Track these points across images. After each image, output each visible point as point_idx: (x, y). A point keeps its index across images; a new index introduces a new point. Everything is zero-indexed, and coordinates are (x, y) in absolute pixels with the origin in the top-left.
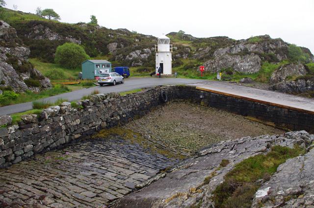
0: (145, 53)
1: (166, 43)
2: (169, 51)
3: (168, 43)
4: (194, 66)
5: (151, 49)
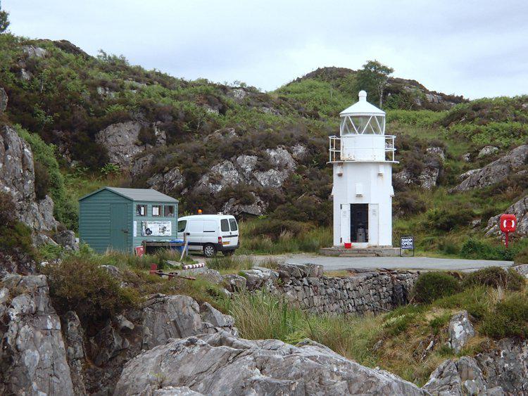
0: (273, 167)
1: (373, 130)
2: (382, 159)
3: (377, 131)
4: (474, 216)
5: (291, 152)
